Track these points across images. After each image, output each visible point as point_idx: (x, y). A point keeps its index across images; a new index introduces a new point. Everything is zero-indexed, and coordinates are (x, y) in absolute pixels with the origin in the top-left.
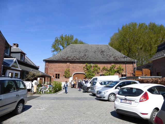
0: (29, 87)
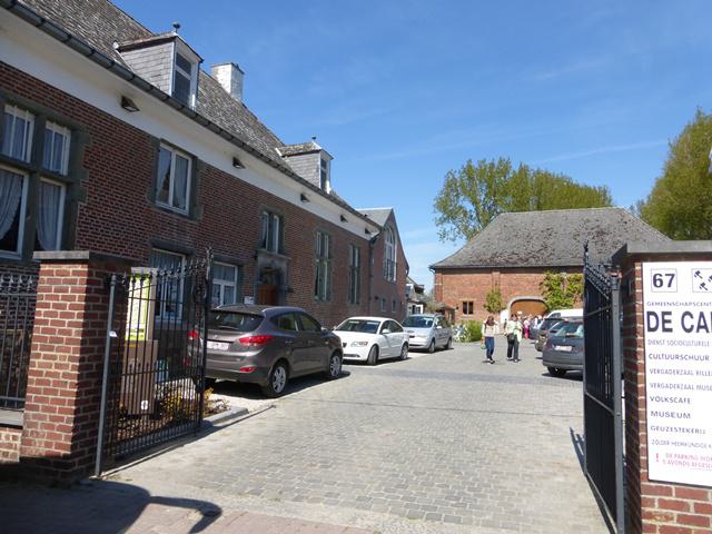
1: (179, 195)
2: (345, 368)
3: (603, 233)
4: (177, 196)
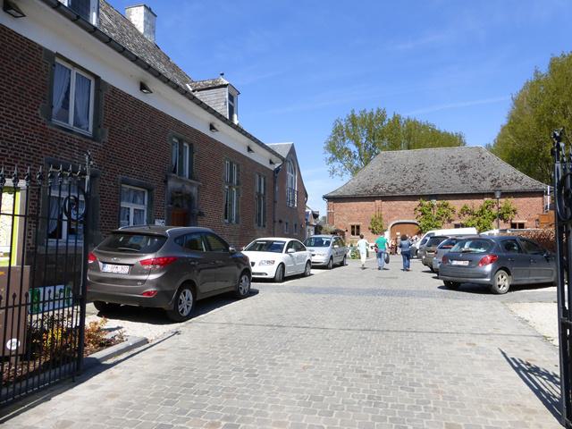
1: (80, 114)
2: (254, 286)
3: (466, 167)
4: (77, 113)
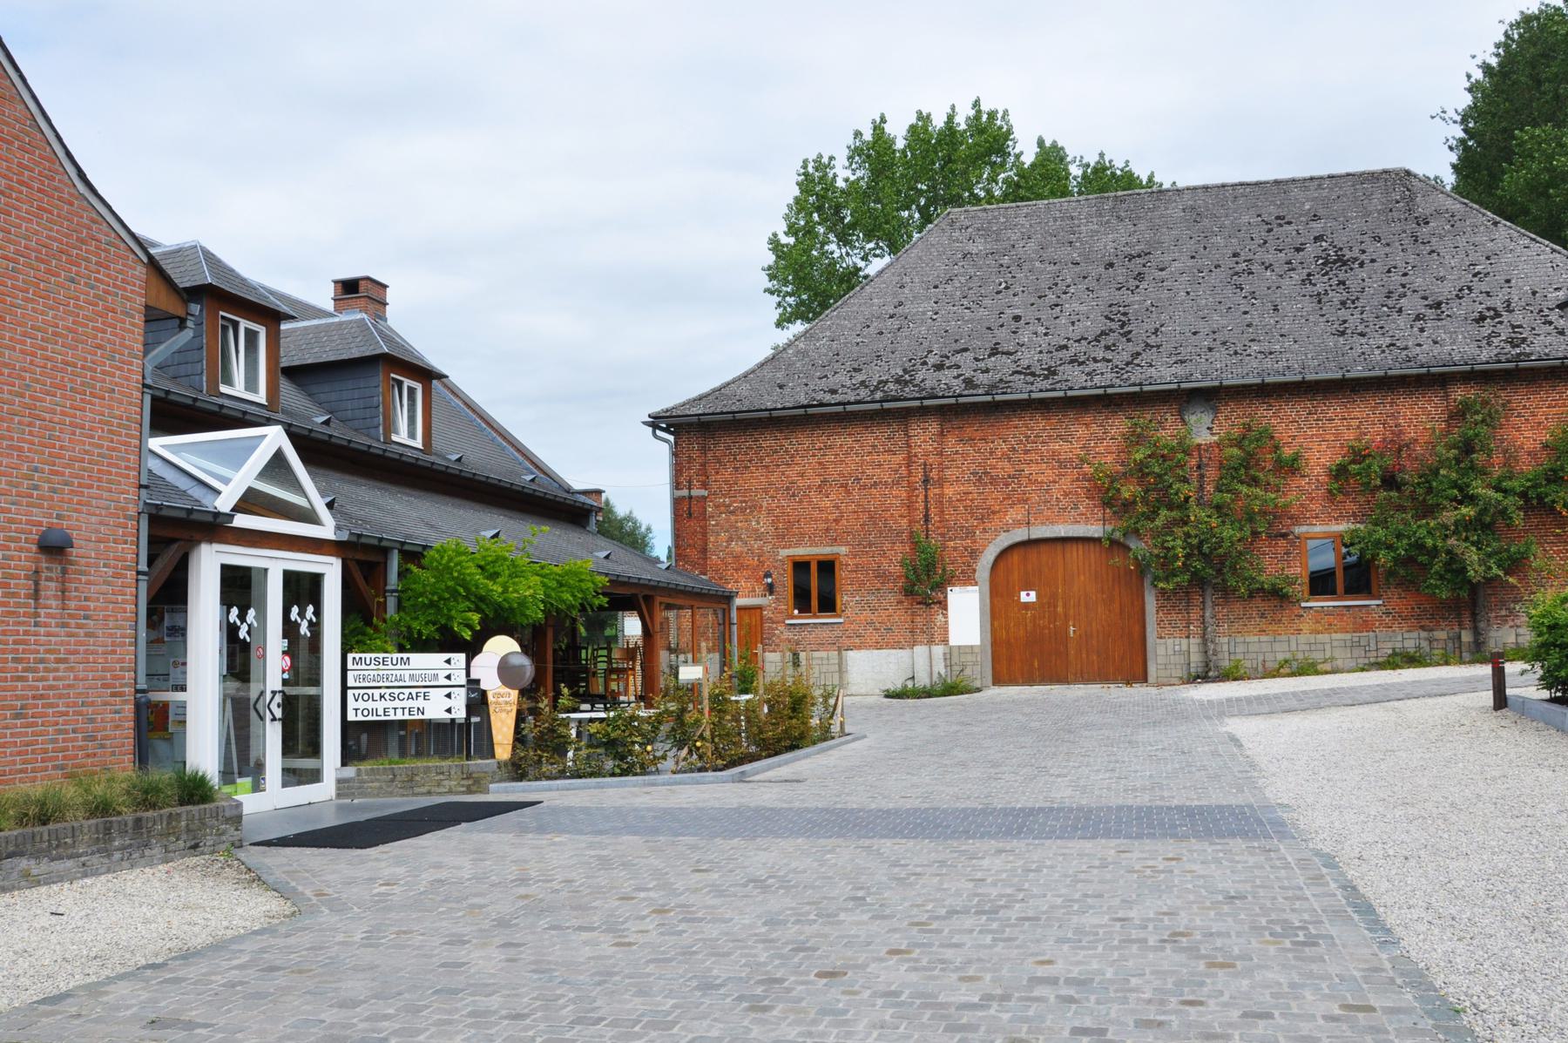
0: (448, 703)
3: (1342, 261)
